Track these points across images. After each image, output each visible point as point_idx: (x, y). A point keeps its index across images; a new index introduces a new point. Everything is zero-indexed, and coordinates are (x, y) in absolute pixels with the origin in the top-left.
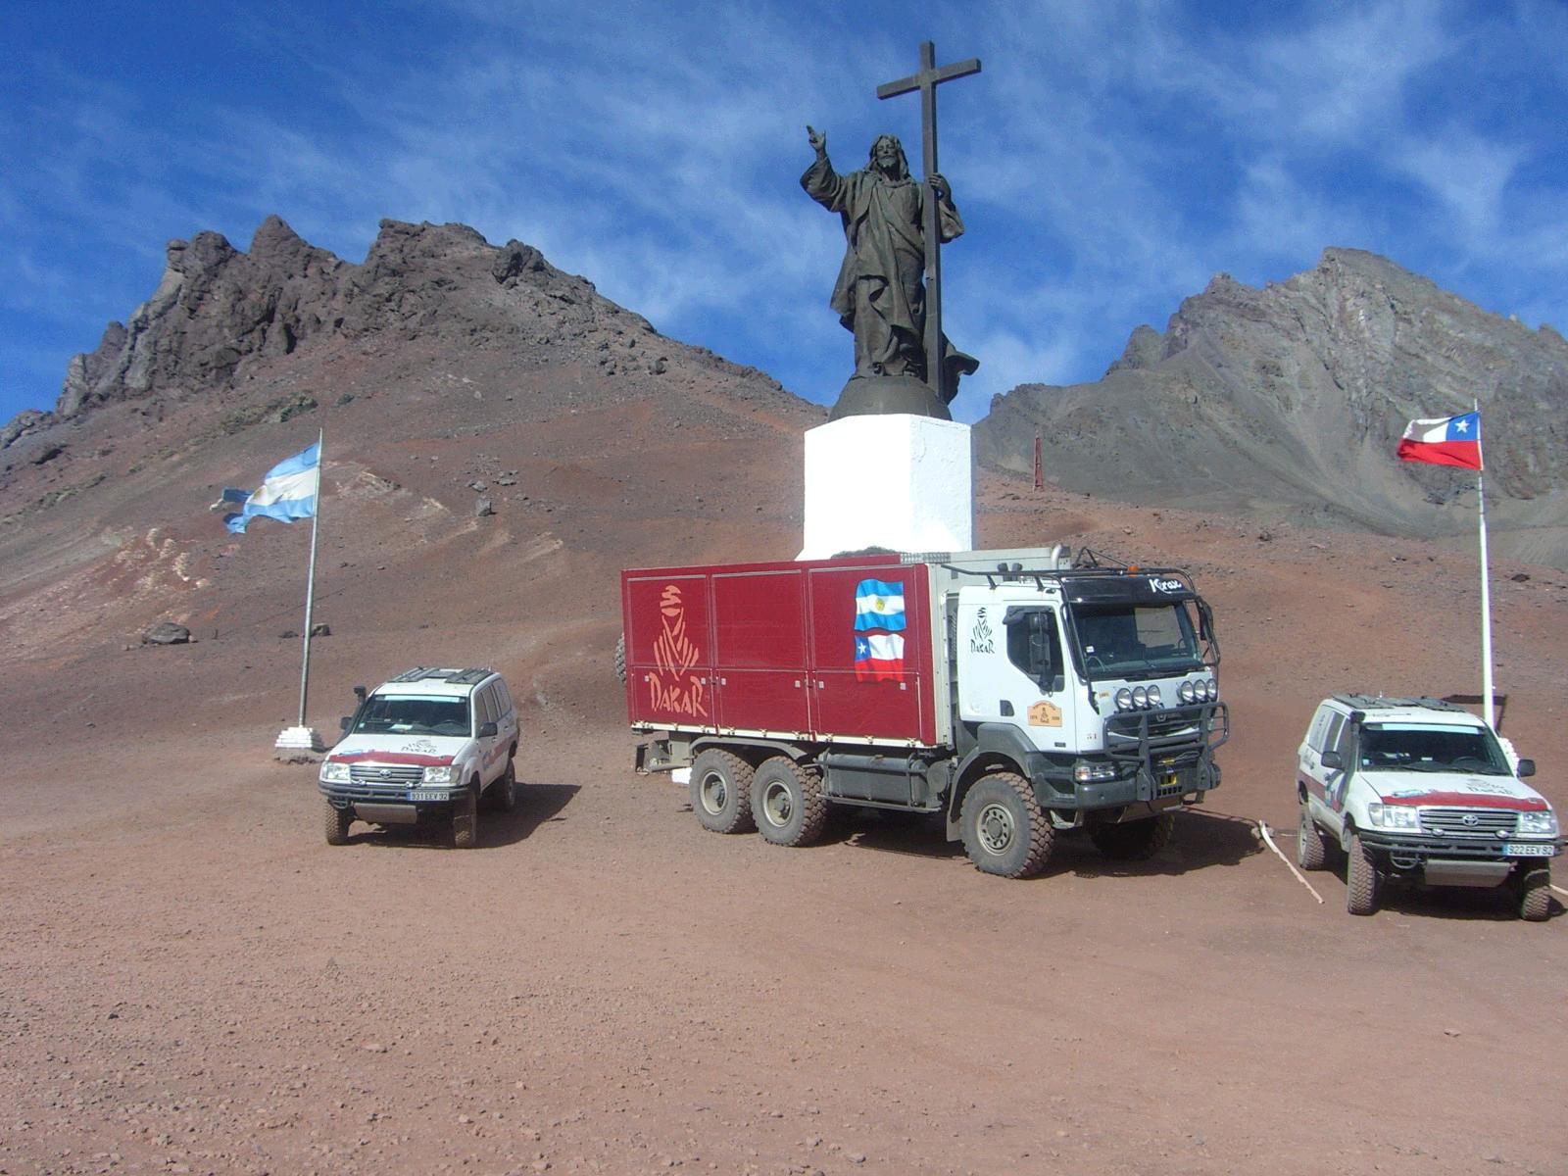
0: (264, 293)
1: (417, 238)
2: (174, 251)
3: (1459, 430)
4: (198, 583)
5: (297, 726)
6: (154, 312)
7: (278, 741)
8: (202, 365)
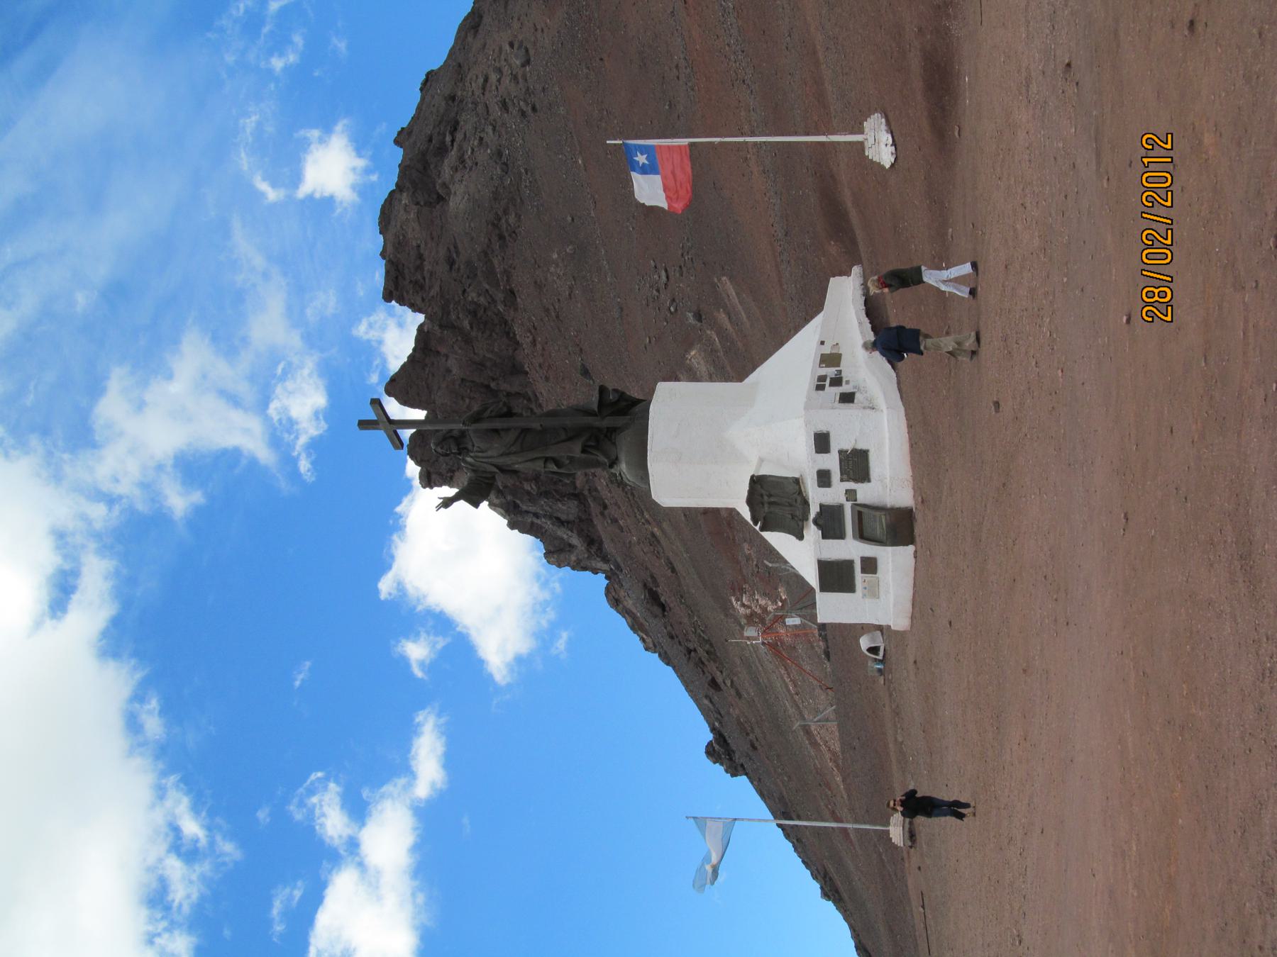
0: (470, 398)
1: (400, 266)
3: (645, 156)
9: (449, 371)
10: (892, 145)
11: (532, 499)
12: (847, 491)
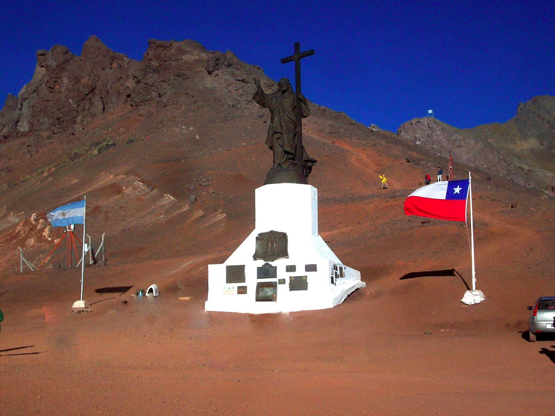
2: (41, 56)
3: (455, 189)
4: (55, 241)
5: (80, 300)
6: (31, 90)
7: (73, 305)
8: (58, 119)
10: (475, 303)
12: (284, 280)
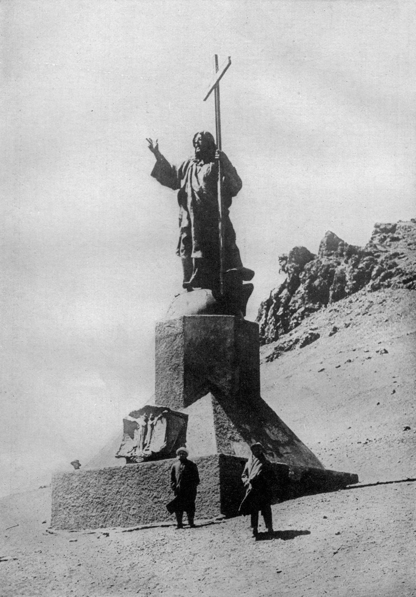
9: (339, 264)
11: (274, 314)
